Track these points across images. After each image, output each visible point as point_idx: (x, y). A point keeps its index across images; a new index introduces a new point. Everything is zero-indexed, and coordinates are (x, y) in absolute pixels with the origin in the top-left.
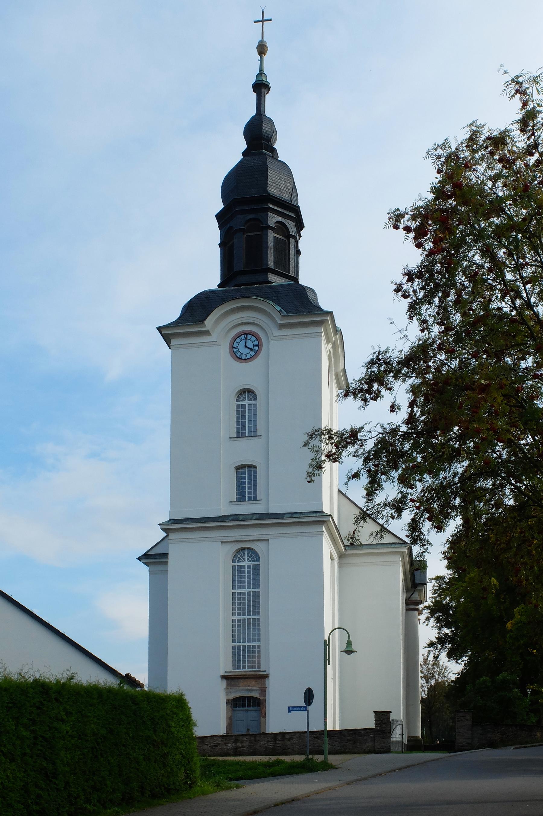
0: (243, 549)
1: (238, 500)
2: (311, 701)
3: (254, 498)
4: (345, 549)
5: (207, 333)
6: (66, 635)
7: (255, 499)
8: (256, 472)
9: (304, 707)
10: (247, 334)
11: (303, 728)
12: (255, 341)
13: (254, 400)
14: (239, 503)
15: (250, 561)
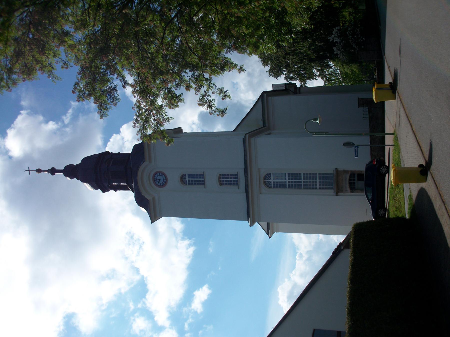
0: (264, 182)
1: (237, 184)
2: (351, 143)
3: (236, 176)
4: (265, 127)
5: (154, 198)
6: (310, 282)
7: (237, 175)
8: (223, 175)
9: (355, 148)
10: (154, 179)
11: (368, 149)
12: (157, 175)
13: (186, 175)
14: (239, 184)
15: (271, 178)
